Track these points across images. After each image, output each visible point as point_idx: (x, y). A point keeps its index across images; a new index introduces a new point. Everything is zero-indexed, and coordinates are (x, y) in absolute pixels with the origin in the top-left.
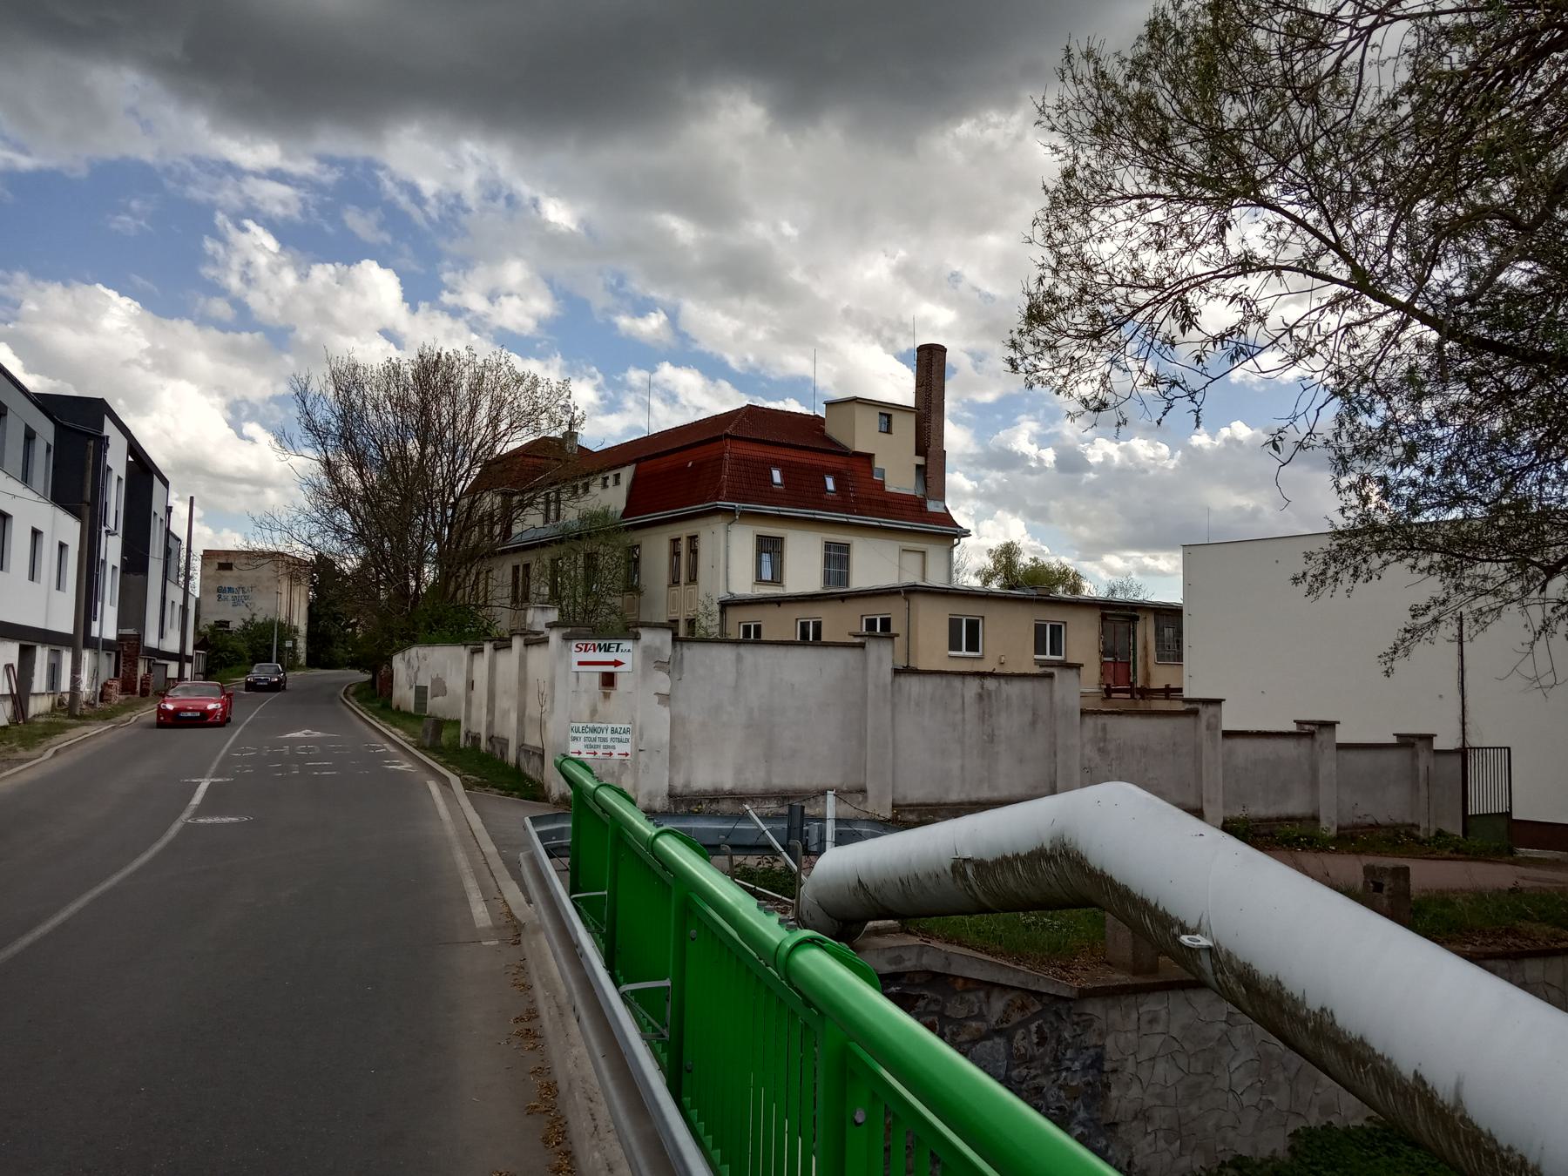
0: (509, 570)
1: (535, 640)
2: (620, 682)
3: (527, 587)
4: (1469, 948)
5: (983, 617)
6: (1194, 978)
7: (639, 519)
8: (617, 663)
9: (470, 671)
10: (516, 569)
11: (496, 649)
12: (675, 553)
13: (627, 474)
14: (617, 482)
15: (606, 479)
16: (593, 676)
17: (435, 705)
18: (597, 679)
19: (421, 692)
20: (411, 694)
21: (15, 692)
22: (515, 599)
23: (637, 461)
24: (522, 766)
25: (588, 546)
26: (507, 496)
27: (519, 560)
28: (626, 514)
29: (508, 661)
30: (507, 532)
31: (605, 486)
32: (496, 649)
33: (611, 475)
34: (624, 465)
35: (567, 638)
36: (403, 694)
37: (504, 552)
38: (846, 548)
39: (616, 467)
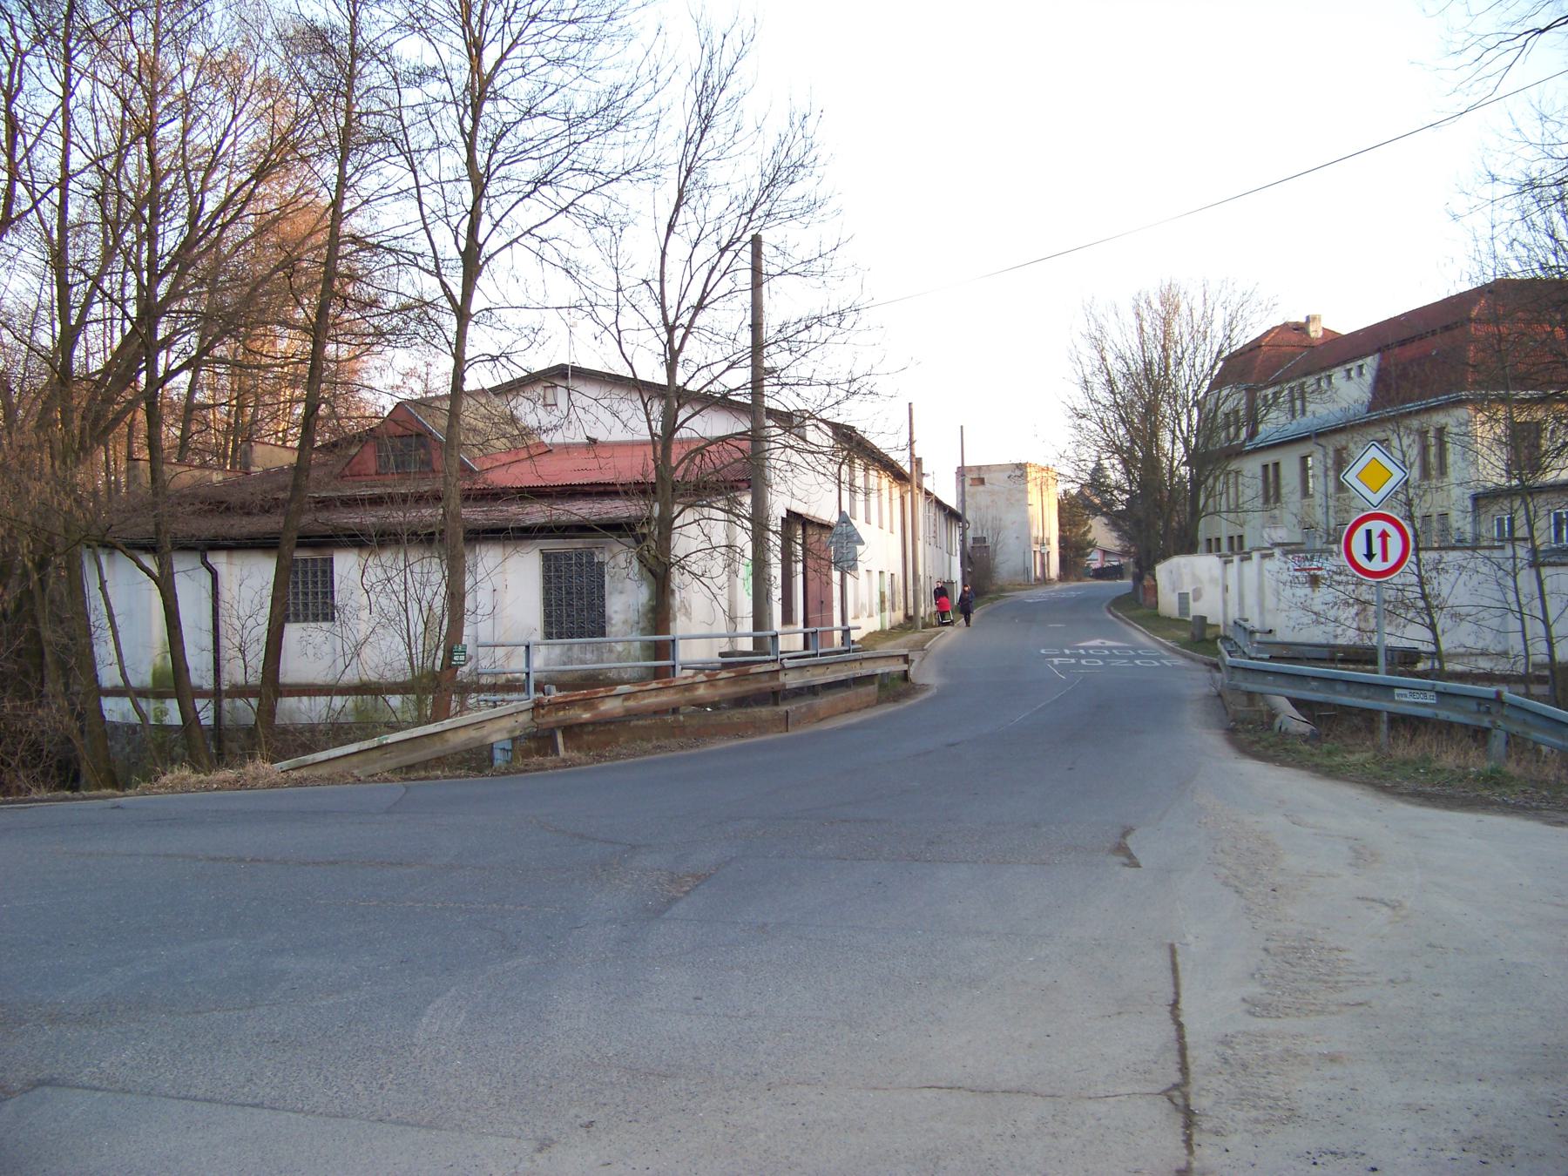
0: (1259, 471)
4: (1139, 612)
6: (61, 108)
9: (1224, 577)
10: (1265, 467)
11: (1242, 560)
13: (1370, 363)
14: (1360, 374)
15: (1349, 371)
17: (1196, 609)
19: (1183, 598)
20: (1175, 599)
21: (836, 575)
22: (1266, 500)
23: (1379, 350)
24: (1294, 696)
25: (1341, 440)
26: (1251, 392)
27: (1270, 458)
28: (1372, 407)
31: (1349, 377)
32: (1242, 560)
33: (1353, 365)
34: (1367, 355)
36: (1168, 602)
37: (1249, 453)
38: (1180, 614)
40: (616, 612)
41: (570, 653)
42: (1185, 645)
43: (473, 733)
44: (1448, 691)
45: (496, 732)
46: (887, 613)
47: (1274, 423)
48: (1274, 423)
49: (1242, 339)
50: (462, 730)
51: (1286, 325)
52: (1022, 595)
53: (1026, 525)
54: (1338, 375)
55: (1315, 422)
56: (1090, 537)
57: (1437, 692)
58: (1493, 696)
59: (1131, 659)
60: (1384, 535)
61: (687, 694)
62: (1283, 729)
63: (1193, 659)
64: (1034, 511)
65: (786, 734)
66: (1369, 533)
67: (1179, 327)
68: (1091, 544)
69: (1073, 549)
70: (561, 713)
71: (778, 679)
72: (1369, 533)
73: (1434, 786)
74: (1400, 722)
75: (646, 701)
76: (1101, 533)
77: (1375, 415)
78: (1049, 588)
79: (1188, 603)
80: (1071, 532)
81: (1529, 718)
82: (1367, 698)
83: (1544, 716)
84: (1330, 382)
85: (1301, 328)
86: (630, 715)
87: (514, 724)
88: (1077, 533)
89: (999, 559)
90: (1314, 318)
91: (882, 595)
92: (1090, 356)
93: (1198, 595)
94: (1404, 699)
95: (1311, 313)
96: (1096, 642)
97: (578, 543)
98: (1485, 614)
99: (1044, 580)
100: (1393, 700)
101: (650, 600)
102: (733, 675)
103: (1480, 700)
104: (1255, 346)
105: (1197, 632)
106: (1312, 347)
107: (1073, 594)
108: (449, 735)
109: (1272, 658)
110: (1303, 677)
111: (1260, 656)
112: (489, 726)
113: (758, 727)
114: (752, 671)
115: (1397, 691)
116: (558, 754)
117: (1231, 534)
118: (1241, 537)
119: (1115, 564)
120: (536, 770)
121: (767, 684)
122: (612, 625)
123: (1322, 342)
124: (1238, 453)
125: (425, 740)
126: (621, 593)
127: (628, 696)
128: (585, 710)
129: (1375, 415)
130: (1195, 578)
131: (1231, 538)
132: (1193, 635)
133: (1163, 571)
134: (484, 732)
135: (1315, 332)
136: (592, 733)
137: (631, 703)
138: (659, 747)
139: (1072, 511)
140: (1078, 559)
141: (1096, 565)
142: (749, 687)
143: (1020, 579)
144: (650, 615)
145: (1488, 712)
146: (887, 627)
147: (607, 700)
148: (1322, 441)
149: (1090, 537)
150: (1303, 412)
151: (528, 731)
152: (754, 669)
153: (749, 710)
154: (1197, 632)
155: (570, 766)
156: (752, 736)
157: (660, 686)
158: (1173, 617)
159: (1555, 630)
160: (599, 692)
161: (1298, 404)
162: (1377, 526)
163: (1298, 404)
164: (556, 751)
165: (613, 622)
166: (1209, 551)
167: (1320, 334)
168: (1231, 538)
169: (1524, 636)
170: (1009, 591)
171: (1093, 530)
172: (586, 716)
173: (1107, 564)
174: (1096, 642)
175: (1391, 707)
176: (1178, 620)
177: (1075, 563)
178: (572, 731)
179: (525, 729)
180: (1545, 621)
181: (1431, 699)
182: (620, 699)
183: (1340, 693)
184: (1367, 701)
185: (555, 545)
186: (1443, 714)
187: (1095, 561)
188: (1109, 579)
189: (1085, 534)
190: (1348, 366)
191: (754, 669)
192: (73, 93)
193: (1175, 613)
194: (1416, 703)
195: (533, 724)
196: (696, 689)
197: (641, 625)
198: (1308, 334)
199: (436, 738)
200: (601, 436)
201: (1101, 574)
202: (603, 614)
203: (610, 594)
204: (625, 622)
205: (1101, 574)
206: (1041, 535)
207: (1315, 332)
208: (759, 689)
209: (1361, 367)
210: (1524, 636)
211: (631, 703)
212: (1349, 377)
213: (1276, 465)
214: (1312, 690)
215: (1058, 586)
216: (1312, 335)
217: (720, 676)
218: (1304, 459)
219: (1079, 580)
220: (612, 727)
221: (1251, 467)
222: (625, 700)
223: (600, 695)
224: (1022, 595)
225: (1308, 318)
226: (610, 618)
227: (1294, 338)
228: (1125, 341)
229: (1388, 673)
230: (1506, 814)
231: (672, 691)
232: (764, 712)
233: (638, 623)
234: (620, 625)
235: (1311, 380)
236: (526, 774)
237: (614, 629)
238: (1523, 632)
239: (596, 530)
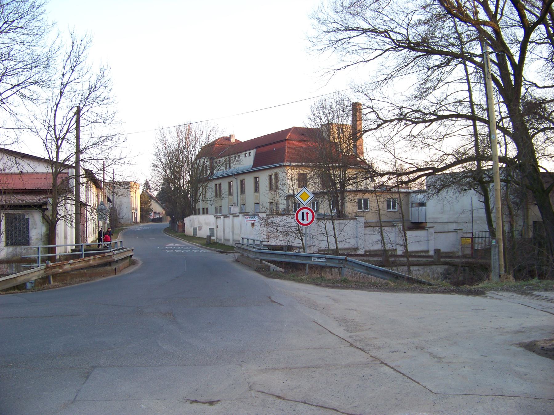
0: (214, 186)
1: (235, 216)
2: (255, 224)
3: (216, 189)
5: (369, 199)
7: (258, 168)
8: (254, 221)
10: (216, 185)
12: (271, 180)
13: (253, 152)
14: (250, 155)
15: (246, 154)
16: (249, 224)
18: (250, 224)
19: (195, 230)
20: (192, 230)
23: (256, 148)
25: (241, 177)
26: (211, 160)
27: (218, 182)
29: (228, 221)
30: (212, 173)
33: (248, 152)
34: (252, 149)
35: (244, 216)
36: (189, 230)
39: (250, 150)
40: (33, 235)
41: (16, 250)
42: (204, 245)
43: (26, 277)
44: (330, 257)
45: (34, 276)
46: (95, 234)
47: (220, 171)
48: (220, 171)
49: (211, 141)
50: (22, 276)
51: (223, 137)
52: (130, 228)
53: (129, 203)
54: (242, 156)
55: (235, 170)
56: (151, 207)
57: (326, 258)
58: (344, 259)
59: (174, 249)
60: (307, 214)
61: (87, 263)
62: (275, 270)
63: (211, 250)
64: (133, 199)
65: (116, 276)
66: (303, 213)
67: (192, 138)
68: (151, 210)
69: (145, 211)
70: (53, 270)
71: (112, 258)
72: (303, 213)
73: (330, 284)
74: (311, 267)
75: (76, 265)
76: (156, 208)
77: (255, 169)
78: (139, 226)
79: (197, 231)
80: (144, 206)
81: (353, 264)
82: (303, 260)
83: (358, 264)
84: (239, 158)
85: (228, 139)
86: (73, 270)
87: (39, 274)
88: (147, 207)
89: (121, 215)
90: (232, 136)
91: (94, 228)
92: (161, 146)
93: (200, 228)
94: (315, 260)
95: (231, 134)
96: (172, 244)
97: (20, 212)
98: (319, 235)
99: (136, 223)
100: (312, 261)
101: (46, 231)
102: (100, 256)
103: (339, 260)
104: (213, 143)
105: (208, 241)
106: (232, 145)
107: (148, 228)
108: (18, 278)
109: (269, 249)
110: (281, 255)
111: (265, 248)
112: (31, 275)
113: (107, 273)
114: (106, 255)
115: (313, 258)
116: (51, 284)
117: (203, 207)
118: (207, 208)
119: (158, 217)
120: (48, 289)
121: (110, 260)
122: (32, 240)
123: (235, 144)
124: (207, 180)
125: (10, 280)
126: (35, 229)
127: (72, 264)
128: (60, 269)
129: (255, 169)
130: (199, 222)
131: (203, 209)
132: (207, 242)
133: (187, 220)
134: (29, 277)
135: (233, 140)
136: (59, 276)
137: (72, 266)
138: (82, 280)
139: (146, 199)
140: (147, 215)
141: (152, 218)
142: (105, 260)
143: (127, 222)
144: (46, 237)
145: (342, 263)
146: (95, 240)
147: (66, 265)
148: (236, 177)
149: (151, 207)
150: (230, 167)
151: (44, 276)
152: (106, 255)
153: (104, 268)
154: (208, 241)
155: (58, 287)
156: (106, 276)
157: (81, 260)
158: (191, 236)
159: (338, 240)
160: (64, 263)
161: (228, 165)
162: (305, 211)
163: (228, 165)
164: (50, 283)
165: (32, 239)
166: (204, 213)
167: (234, 141)
168: (203, 209)
169: (328, 242)
170: (125, 227)
171: (152, 205)
172: (61, 271)
173: (155, 217)
174: (172, 244)
175: (309, 262)
176: (193, 237)
177: (146, 217)
178: (55, 276)
179: (43, 275)
180: (335, 237)
181: (324, 260)
182: (69, 265)
183: (293, 259)
184: (303, 261)
185: (11, 212)
186: (328, 264)
187: (152, 216)
188: (158, 222)
189: (149, 206)
190: (246, 152)
191: (106, 255)
192: (365, 160)
193: (192, 234)
194: (319, 261)
195: (45, 274)
196: (90, 261)
197: (43, 240)
198: (230, 141)
199: (14, 280)
200: (24, 171)
201: (154, 220)
202: (28, 236)
203: (31, 229)
204: (37, 239)
205: (154, 220)
206: (135, 207)
207: (233, 140)
208: (108, 261)
209: (250, 153)
210: (328, 242)
211: (72, 266)
212: (246, 156)
213: (220, 184)
214: (284, 258)
215: (141, 225)
216: (232, 141)
217: (97, 257)
218: (230, 183)
219: (147, 223)
220: (65, 274)
221: (212, 185)
222: (71, 265)
223: (65, 263)
224: (130, 228)
225: (230, 135)
226: (31, 238)
227: (226, 142)
228: (173, 142)
229: (84, 254)
230: (356, 290)
231: (84, 262)
232: (108, 268)
233: (42, 239)
234: (35, 240)
235: (233, 157)
236: (44, 291)
237: (32, 241)
238: (328, 240)
239: (32, 207)
